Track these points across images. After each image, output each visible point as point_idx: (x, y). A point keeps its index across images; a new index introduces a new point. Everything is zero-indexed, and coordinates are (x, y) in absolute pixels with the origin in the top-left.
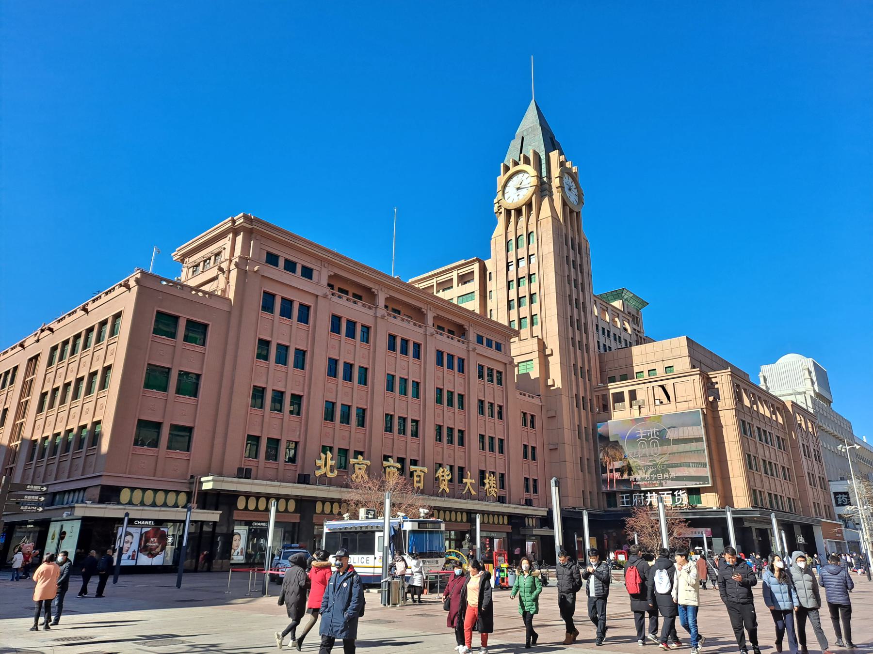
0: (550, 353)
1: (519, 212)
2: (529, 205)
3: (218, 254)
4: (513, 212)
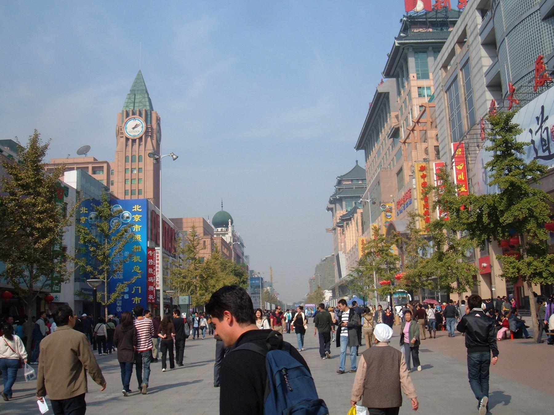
1: (134, 141)
2: (141, 139)
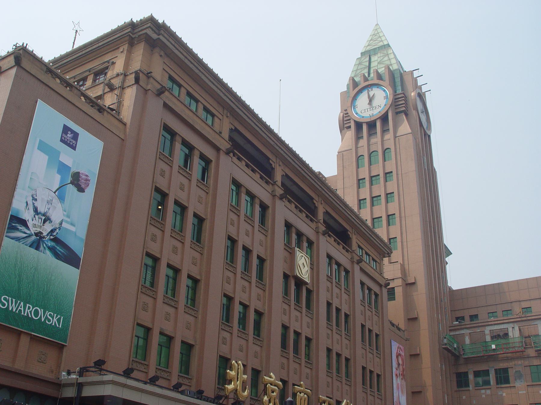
0: (413, 281)
1: (372, 125)
2: (384, 118)
3: (103, 72)
4: (365, 127)
